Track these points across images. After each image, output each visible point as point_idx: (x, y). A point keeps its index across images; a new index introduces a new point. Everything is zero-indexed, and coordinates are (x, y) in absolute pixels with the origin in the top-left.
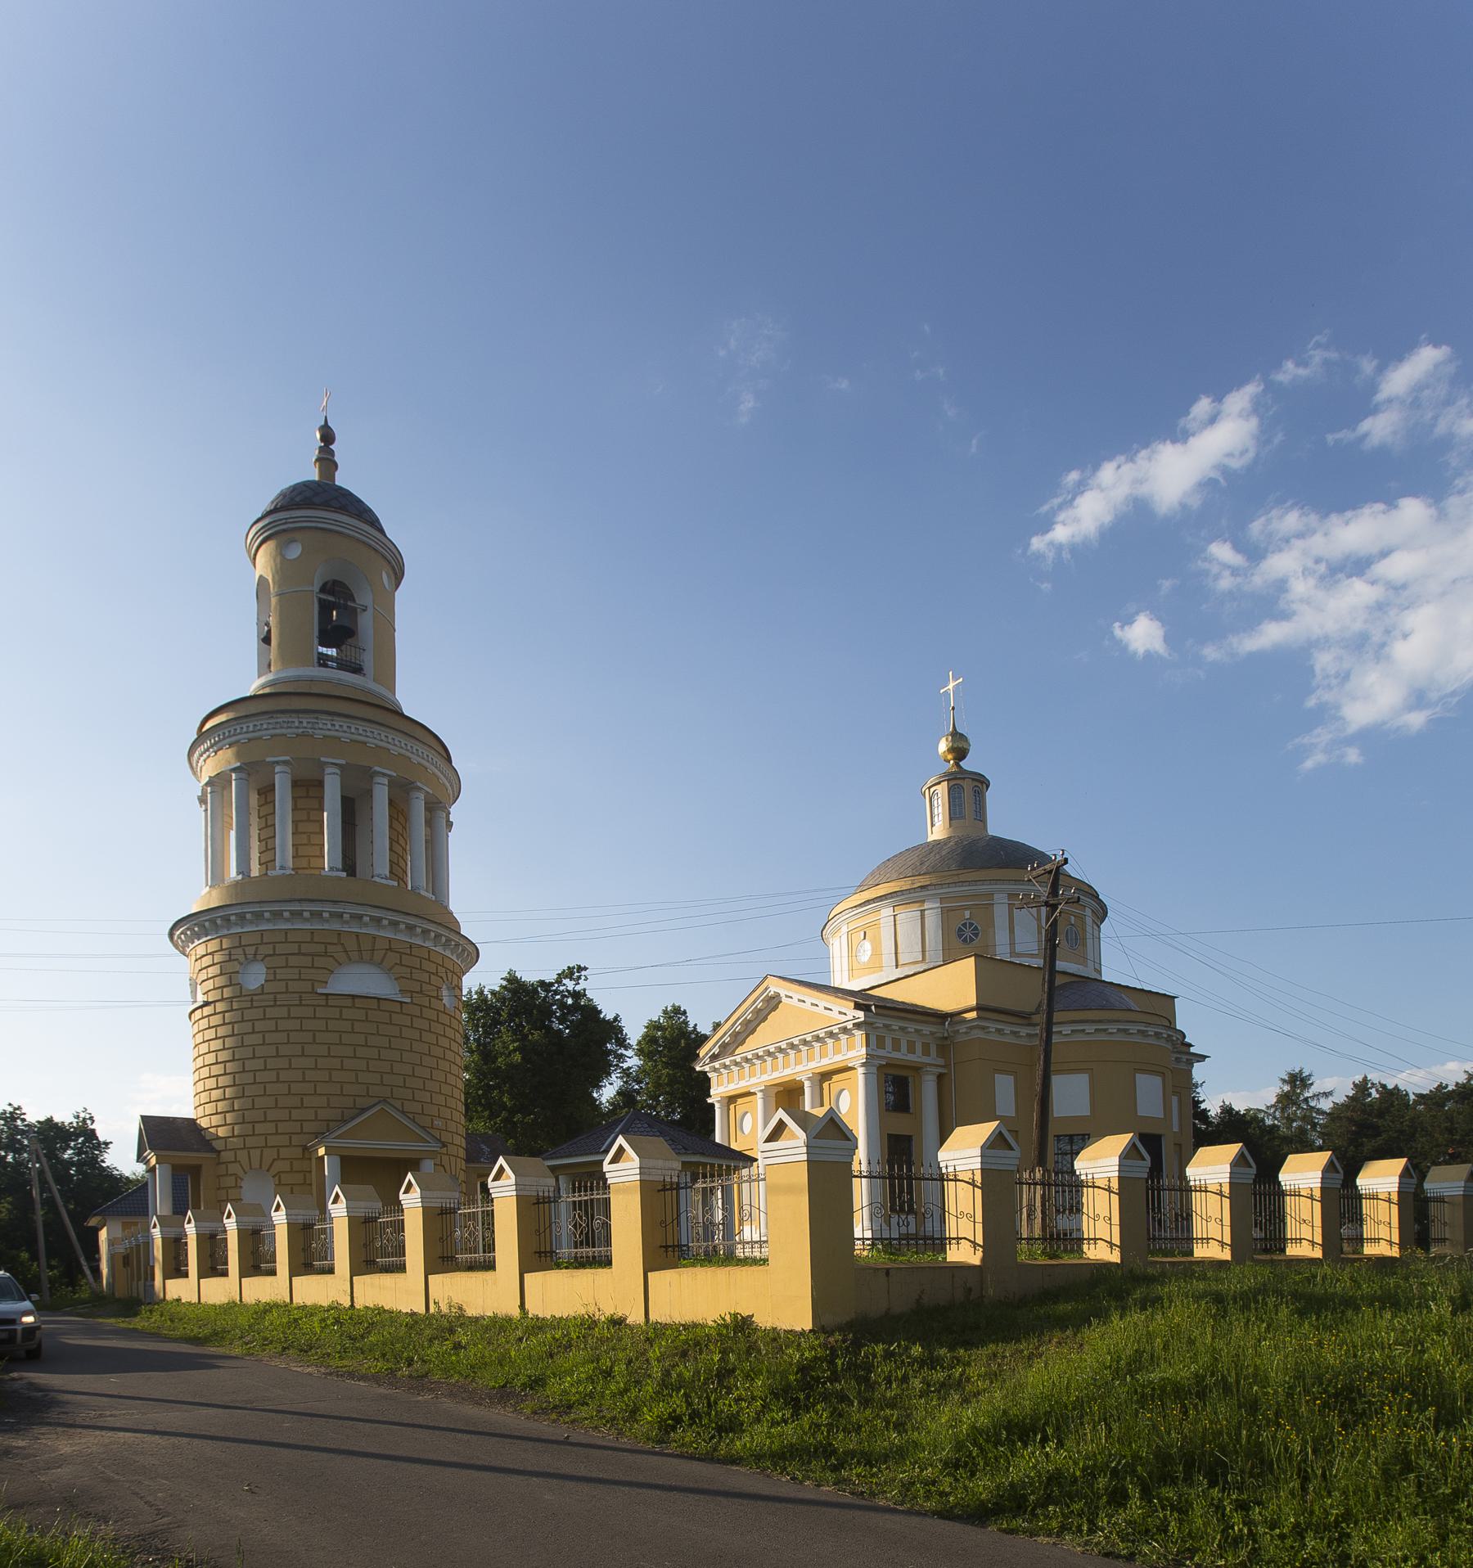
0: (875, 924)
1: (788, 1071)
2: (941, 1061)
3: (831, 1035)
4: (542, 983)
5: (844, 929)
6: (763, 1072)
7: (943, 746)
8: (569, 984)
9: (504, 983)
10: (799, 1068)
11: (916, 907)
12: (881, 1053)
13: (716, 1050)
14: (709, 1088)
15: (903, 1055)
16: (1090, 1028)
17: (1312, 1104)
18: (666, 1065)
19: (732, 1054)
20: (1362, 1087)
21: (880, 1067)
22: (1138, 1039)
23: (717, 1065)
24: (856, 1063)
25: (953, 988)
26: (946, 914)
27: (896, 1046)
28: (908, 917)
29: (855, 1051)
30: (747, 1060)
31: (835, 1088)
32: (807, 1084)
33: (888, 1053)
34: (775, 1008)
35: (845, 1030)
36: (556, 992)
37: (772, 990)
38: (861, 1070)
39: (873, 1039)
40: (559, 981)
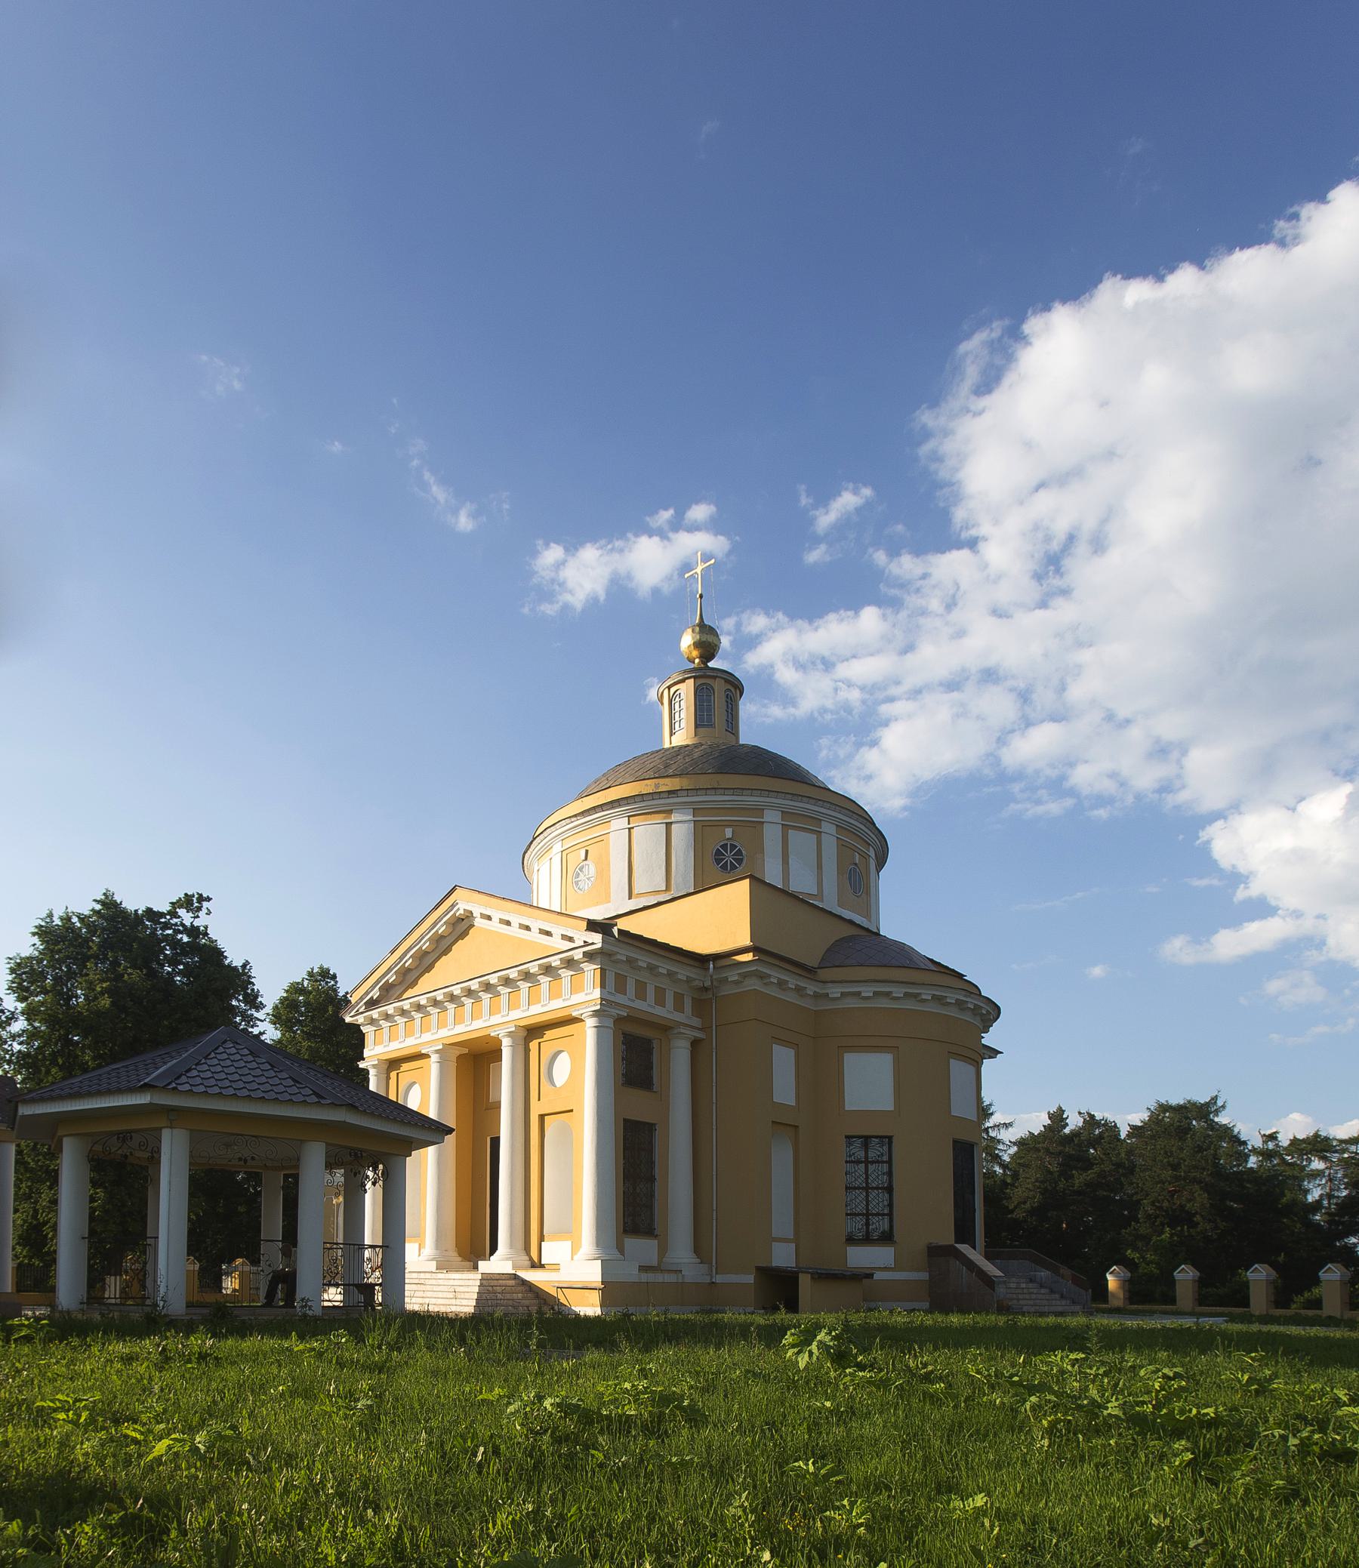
0: (600, 839)
1: (478, 1024)
2: (696, 1022)
3: (548, 970)
4: (150, 912)
5: (557, 847)
6: (441, 1025)
7: (687, 640)
8: (186, 917)
9: (98, 907)
10: (496, 1019)
11: (659, 818)
12: (620, 999)
13: (375, 994)
14: (363, 1046)
15: (647, 1006)
16: (898, 991)
17: (992, 1134)
18: (308, 1036)
19: (399, 999)
20: (1058, 1118)
21: (619, 1020)
22: (953, 1012)
23: (375, 1014)
24: (585, 1012)
25: (717, 921)
26: (700, 833)
27: (641, 994)
28: (649, 832)
29: (584, 994)
30: (419, 1008)
31: (548, 1049)
32: (506, 1043)
33: (627, 999)
34: (464, 935)
35: (570, 963)
36: (166, 926)
37: (461, 908)
38: (591, 1023)
39: (611, 978)
40: (173, 914)
